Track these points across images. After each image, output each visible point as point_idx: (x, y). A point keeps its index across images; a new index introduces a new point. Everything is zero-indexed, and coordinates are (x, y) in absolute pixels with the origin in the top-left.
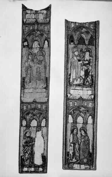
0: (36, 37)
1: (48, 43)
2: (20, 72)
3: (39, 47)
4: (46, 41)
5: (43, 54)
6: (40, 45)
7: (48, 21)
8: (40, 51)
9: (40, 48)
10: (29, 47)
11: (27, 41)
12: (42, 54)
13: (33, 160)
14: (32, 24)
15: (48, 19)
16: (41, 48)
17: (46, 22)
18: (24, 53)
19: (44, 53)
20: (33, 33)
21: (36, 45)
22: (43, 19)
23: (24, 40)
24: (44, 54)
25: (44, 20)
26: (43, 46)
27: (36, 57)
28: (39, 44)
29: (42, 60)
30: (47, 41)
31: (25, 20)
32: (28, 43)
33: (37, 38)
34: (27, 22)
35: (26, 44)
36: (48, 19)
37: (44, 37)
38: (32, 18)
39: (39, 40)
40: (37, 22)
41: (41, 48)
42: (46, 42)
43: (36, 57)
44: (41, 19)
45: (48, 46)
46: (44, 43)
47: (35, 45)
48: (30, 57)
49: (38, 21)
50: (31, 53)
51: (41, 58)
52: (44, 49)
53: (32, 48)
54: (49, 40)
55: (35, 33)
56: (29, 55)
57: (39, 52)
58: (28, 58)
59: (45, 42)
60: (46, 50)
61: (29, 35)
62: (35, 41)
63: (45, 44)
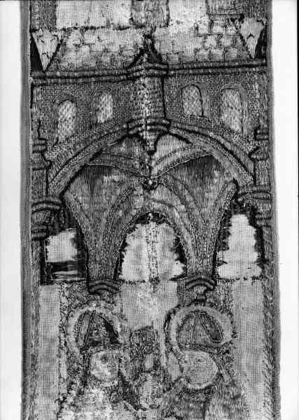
0: (148, 189)
1: (259, 235)
2: (20, 358)
3: (178, 269)
4: (240, 222)
5: (216, 337)
6: (182, 259)
7: (252, 44)
8: (182, 313)
9: (187, 280)
10: (96, 277)
11: (72, 223)
12: (203, 337)
13: (265, 49)
14: (119, 76)
15: (250, 28)
16: (200, 287)
17: (234, 53)
18: (50, 323)
19: (222, 320)
20: (123, 148)
21: (147, 253)
22: (204, 29)
23: (47, 215)
24: (227, 336)
25: (211, 41)
26: (216, 262)
27: (156, 365)
28: (180, 251)
29: (209, 390)
30: (252, 222)
31: (47, 47)
32: (79, 242)
33: (156, 195)
34: (73, 58)
35: (62, 247)
36: (250, 28)
37: (216, 191)
38: (108, 25)
39: (178, 213)
40: (156, 57)
41: (200, 287)
42: (241, 226)
43: (156, 365)
44: (186, 27)
45: (262, 261)
46: (221, 240)
47: (139, 256)
48: (101, 369)
49: (162, 48)
50: (109, 327)
51: (204, 368)
52: (220, 290)
53: (111, 284)
54: (262, 208)
55: (137, 150)
56: (90, 344)
57: (176, 321)
58: (87, 378)
59: (233, 230)
60: (248, 299)
61: (91, 172)
62: (142, 219)
63: (232, 241)
